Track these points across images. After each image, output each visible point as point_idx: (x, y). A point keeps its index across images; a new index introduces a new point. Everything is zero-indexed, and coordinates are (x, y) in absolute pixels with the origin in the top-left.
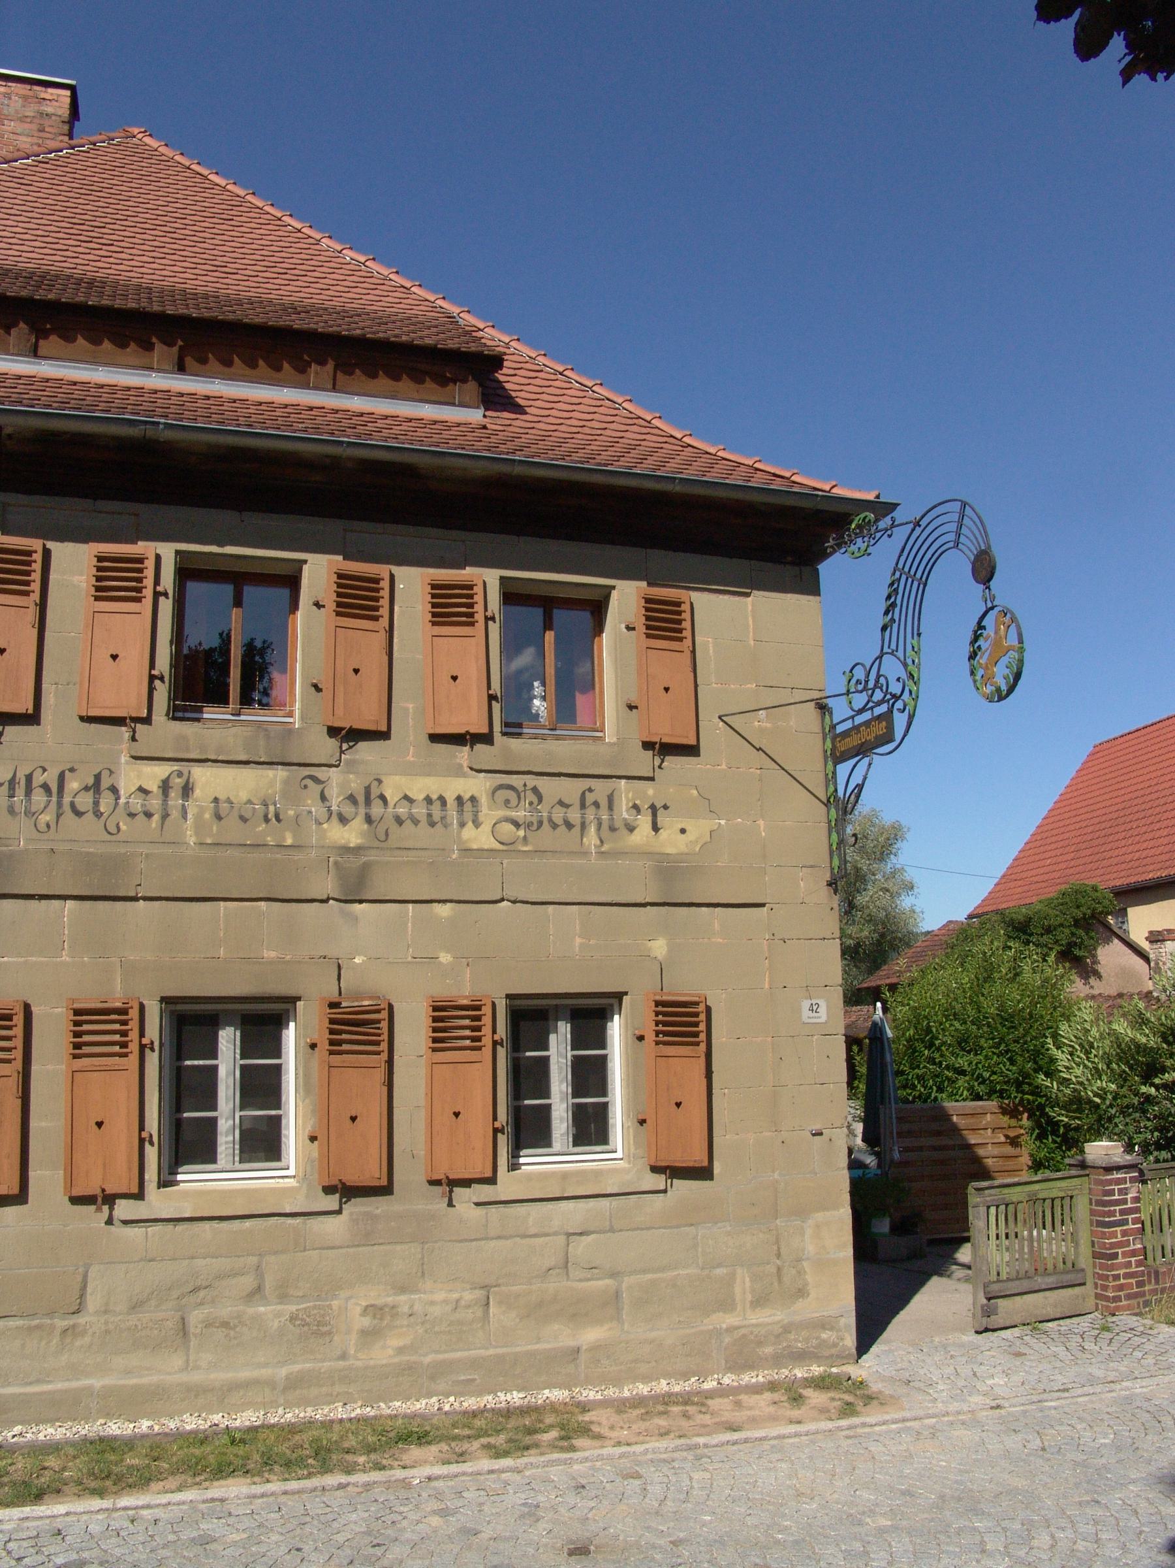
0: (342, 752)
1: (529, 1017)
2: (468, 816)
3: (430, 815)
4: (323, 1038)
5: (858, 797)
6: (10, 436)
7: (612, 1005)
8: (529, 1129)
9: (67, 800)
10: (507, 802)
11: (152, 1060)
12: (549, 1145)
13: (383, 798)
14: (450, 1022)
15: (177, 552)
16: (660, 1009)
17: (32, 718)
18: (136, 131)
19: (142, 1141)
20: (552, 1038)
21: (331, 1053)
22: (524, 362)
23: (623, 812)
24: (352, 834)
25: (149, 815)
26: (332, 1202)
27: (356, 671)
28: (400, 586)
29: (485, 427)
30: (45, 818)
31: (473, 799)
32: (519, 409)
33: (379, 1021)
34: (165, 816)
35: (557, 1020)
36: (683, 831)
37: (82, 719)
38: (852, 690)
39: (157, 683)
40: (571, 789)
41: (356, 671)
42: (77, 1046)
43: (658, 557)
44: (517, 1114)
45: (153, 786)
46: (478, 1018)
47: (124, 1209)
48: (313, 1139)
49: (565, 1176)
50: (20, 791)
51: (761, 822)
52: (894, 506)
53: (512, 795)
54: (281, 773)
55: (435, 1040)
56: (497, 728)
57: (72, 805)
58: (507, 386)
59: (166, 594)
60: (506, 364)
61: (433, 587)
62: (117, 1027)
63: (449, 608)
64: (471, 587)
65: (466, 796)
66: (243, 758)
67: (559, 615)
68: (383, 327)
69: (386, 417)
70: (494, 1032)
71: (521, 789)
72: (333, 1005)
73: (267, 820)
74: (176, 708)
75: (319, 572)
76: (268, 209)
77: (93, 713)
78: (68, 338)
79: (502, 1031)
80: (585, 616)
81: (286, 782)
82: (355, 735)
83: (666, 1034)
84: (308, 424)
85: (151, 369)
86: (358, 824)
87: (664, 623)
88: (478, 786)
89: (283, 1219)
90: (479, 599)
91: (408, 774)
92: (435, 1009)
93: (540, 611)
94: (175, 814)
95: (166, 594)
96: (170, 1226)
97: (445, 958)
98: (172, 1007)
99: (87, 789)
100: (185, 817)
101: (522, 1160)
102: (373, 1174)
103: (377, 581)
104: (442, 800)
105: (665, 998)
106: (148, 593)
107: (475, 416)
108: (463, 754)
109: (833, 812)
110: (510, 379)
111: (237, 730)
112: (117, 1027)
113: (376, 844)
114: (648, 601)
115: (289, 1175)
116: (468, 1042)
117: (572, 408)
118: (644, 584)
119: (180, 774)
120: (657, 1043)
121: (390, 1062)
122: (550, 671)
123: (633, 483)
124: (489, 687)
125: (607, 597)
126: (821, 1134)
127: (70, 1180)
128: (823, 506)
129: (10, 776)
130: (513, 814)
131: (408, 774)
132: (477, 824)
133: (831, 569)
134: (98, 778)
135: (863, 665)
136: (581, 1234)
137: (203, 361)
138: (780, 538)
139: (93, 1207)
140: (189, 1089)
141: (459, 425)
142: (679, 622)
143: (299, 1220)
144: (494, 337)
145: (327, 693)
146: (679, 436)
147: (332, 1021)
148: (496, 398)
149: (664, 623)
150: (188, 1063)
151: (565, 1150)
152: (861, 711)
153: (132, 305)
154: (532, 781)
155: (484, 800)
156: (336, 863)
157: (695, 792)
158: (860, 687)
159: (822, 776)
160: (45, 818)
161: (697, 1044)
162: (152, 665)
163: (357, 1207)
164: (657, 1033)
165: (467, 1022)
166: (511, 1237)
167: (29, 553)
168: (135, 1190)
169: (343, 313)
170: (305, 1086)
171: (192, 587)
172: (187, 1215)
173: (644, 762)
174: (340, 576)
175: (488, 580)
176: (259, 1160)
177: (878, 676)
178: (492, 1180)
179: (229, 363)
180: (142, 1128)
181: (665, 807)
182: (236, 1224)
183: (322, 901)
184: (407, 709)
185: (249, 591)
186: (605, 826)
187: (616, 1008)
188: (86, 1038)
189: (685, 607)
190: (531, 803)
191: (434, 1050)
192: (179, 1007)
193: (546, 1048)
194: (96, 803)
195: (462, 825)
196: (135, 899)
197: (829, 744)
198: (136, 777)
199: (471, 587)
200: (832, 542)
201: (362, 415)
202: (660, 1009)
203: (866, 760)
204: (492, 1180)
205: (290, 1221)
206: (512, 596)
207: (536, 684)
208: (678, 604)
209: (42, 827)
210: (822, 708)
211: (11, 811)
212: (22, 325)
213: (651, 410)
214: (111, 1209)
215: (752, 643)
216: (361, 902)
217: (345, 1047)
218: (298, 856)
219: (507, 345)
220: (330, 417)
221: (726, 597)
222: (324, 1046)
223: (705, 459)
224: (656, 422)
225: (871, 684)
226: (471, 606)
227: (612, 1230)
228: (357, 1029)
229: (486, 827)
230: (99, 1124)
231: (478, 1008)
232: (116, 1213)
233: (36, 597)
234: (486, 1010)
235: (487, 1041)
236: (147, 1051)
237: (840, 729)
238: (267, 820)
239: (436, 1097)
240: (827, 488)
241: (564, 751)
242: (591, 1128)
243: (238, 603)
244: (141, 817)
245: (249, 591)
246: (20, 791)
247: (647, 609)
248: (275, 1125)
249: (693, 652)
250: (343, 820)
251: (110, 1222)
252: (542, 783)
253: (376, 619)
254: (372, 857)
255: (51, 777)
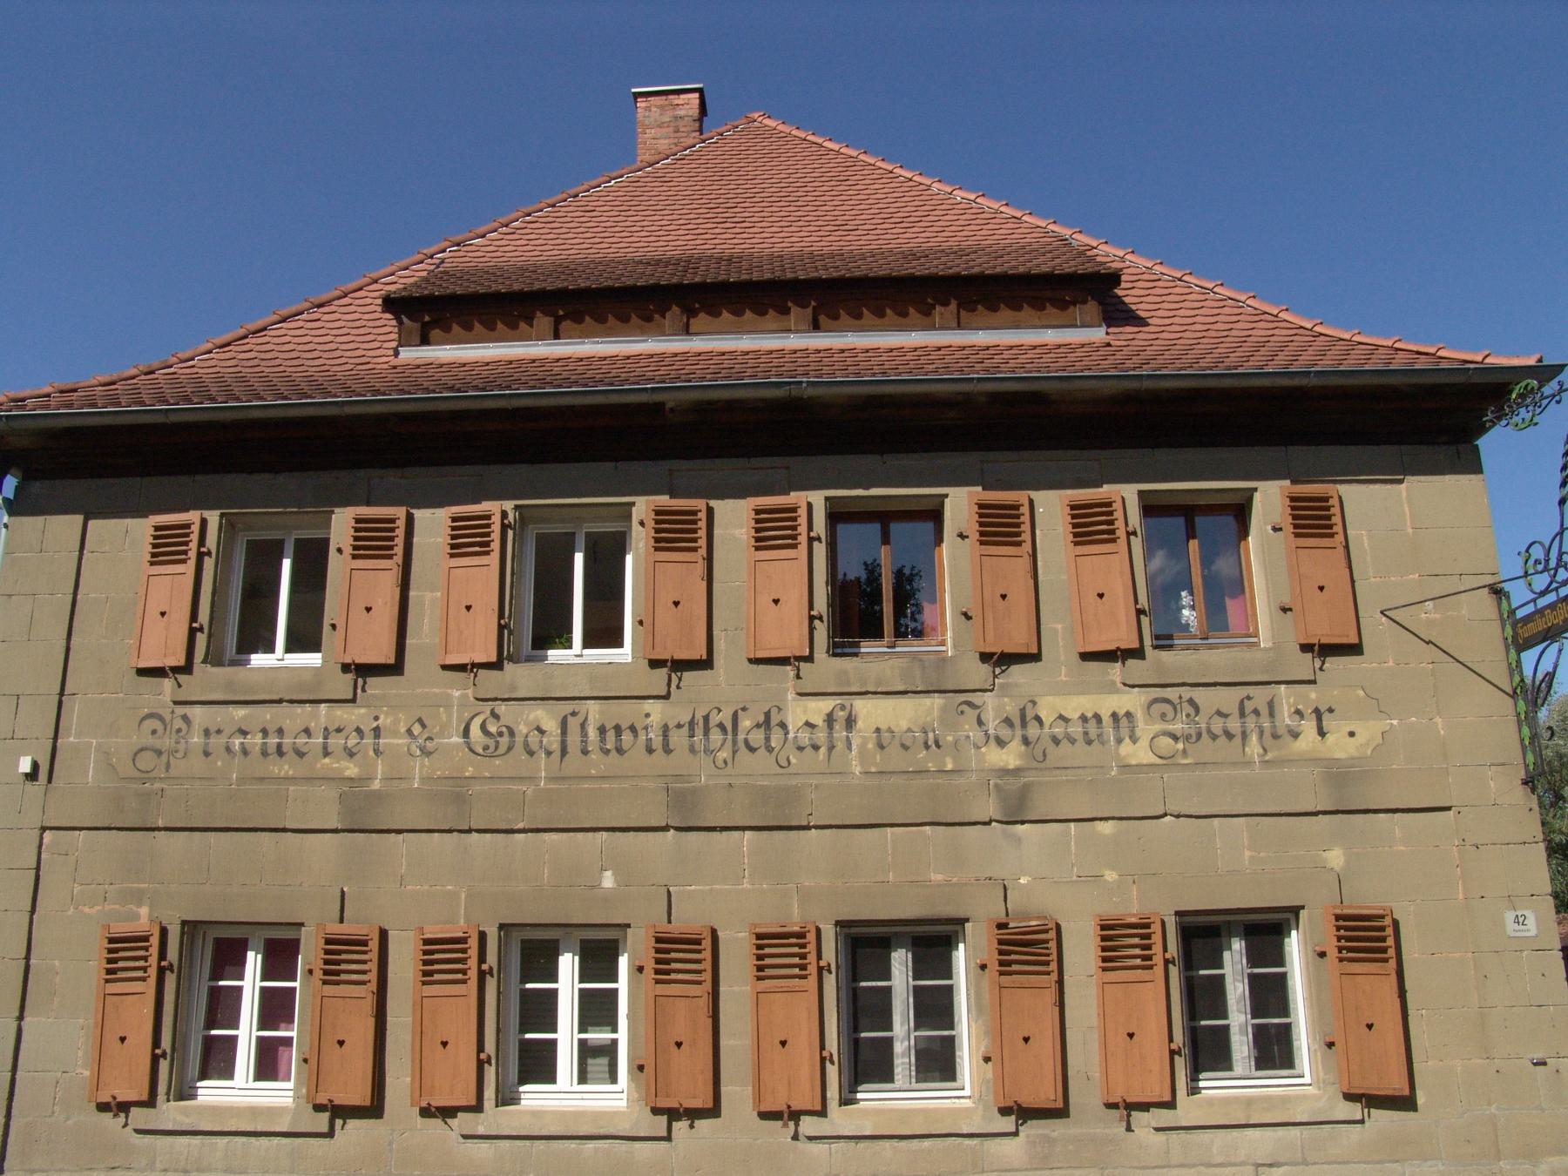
0: (995, 676)
1: (1201, 935)
2: (1125, 732)
3: (1086, 733)
4: (993, 959)
5: (1550, 687)
6: (672, 410)
7: (1288, 920)
8: (1207, 1051)
9: (741, 737)
10: (1163, 715)
11: (830, 981)
12: (1230, 1068)
13: (1038, 719)
14: (1119, 941)
15: (827, 499)
16: (1341, 923)
17: (706, 664)
18: (756, 115)
19: (823, 1060)
20: (1226, 955)
21: (1001, 973)
22: (1141, 273)
23: (1285, 718)
24: (1010, 757)
25: (816, 748)
26: (1008, 1123)
27: (1004, 597)
28: (1039, 510)
29: (1109, 345)
30: (722, 755)
31: (1128, 715)
32: (1142, 322)
33: (1047, 941)
34: (831, 748)
35: (1230, 936)
36: (1352, 734)
37: (751, 661)
38: (1531, 571)
39: (817, 622)
40: (1228, 699)
41: (1004, 597)
42: (760, 969)
43: (1298, 452)
44: (1194, 1034)
45: (819, 721)
46: (1148, 936)
47: (808, 1125)
48: (987, 1059)
49: (1249, 1102)
50: (699, 731)
51: (1438, 720)
52: (1559, 369)
53: (1167, 708)
54: (937, 701)
55: (1104, 960)
56: (1148, 642)
57: (746, 742)
58: (1127, 300)
59: (819, 539)
60: (1123, 278)
61: (1073, 508)
62: (796, 950)
63: (1090, 526)
64: (1109, 504)
65: (1122, 712)
66: (901, 688)
67: (1200, 521)
68: (1000, 261)
69: (1011, 348)
70: (1165, 950)
71: (1176, 701)
72: (1002, 926)
73: (927, 747)
74: (835, 645)
75: (960, 504)
76: (879, 164)
77: (760, 655)
78: (715, 314)
79: (1173, 949)
80: (1229, 521)
81: (944, 709)
82: (1006, 660)
83: (1350, 950)
84: (938, 364)
85: (789, 331)
86: (1015, 746)
87: (1313, 520)
88: (1132, 701)
89: (960, 1140)
90: (1118, 514)
91: (1062, 694)
92: (1103, 928)
93: (1181, 521)
94: (840, 745)
95: (819, 539)
96: (852, 1144)
97: (1110, 876)
98: (846, 930)
99: (758, 726)
100: (850, 749)
101: (1201, 1084)
102: (1046, 1094)
103: (1017, 507)
104: (1097, 717)
105: (1346, 911)
106: (803, 539)
107: (1098, 334)
108: (1115, 671)
109: (1521, 704)
110: (1129, 293)
111: (894, 662)
112: (796, 950)
113: (1035, 764)
114: (1293, 499)
115: (966, 1093)
116: (1138, 961)
117: (1199, 314)
118: (1288, 482)
119: (843, 707)
120: (1341, 960)
121: (1060, 982)
122: (1197, 580)
123: (1266, 382)
124: (1136, 602)
125: (1250, 499)
126: (1545, 1064)
127: (758, 1097)
128: (1476, 379)
129: (689, 718)
130: (1170, 727)
131: (1062, 694)
132: (1134, 739)
133: (1493, 443)
134: (768, 715)
135: (1541, 544)
136: (1271, 1165)
137: (836, 317)
138: (1432, 419)
139: (780, 1123)
140: (866, 1010)
141: (1083, 346)
142: (1329, 518)
143: (976, 1141)
144: (1109, 254)
145: (977, 620)
146: (1309, 326)
147: (1000, 942)
148: (1118, 314)
149: (1313, 520)
150: (863, 984)
151: (1247, 1073)
152: (1543, 593)
153: (768, 276)
154: (1186, 693)
155: (1139, 715)
156: (996, 785)
157: (1361, 693)
158: (1540, 567)
159: (1505, 664)
160: (722, 755)
161: (1386, 960)
162: (811, 607)
163: (1032, 1129)
164: (1340, 950)
165: (1136, 941)
166: (1195, 1165)
167: (694, 513)
168: (818, 1107)
169: (960, 253)
170: (977, 1007)
171: (841, 528)
172: (868, 1133)
173: (1304, 665)
174: (981, 506)
175: (1126, 495)
176: (934, 1080)
177: (1561, 554)
178: (1171, 1105)
179: (859, 316)
180: (822, 1047)
181: (1331, 710)
182: (915, 1143)
183: (985, 824)
184: (1056, 631)
185: (895, 527)
186: (1267, 733)
187: (1293, 924)
188: (768, 961)
189: (1334, 502)
190: (1188, 715)
191: (1104, 969)
192: (854, 930)
193: (1221, 966)
194: (768, 739)
195: (1119, 741)
196: (807, 828)
197: (1509, 631)
198: (803, 713)
199: (1109, 504)
200: (1490, 416)
201: (988, 348)
202: (1341, 923)
203: (1555, 646)
204: (1171, 1105)
205: (967, 1142)
206: (1151, 507)
207: (1184, 594)
208: (1326, 499)
209: (720, 763)
210: (1497, 592)
211: (692, 750)
212: (675, 308)
213: (1277, 304)
214: (797, 1125)
215: (1410, 531)
216: (1023, 822)
217: (1015, 967)
218: (960, 781)
219: (1122, 259)
220: (958, 355)
221: (1377, 486)
222: (994, 966)
223: (1340, 346)
224: (1283, 315)
225: (1552, 564)
226: (1111, 523)
227: (1305, 1163)
228: (1026, 949)
229: (1144, 742)
230: (783, 1043)
231: (1147, 926)
232: (801, 1129)
233: (703, 552)
234: (1156, 928)
235: (1158, 960)
236: (825, 973)
237: (1520, 614)
238: (927, 747)
239: (1111, 1020)
240: (1479, 359)
241: (1217, 660)
242: (1274, 1050)
243: (886, 540)
244: (809, 750)
245: (895, 527)
246: (699, 731)
247: (1293, 508)
248: (949, 1044)
249: (1347, 547)
250: (1001, 743)
251: (795, 1137)
252: (1199, 695)
253: (1019, 544)
254: (1030, 778)
255: (725, 717)
